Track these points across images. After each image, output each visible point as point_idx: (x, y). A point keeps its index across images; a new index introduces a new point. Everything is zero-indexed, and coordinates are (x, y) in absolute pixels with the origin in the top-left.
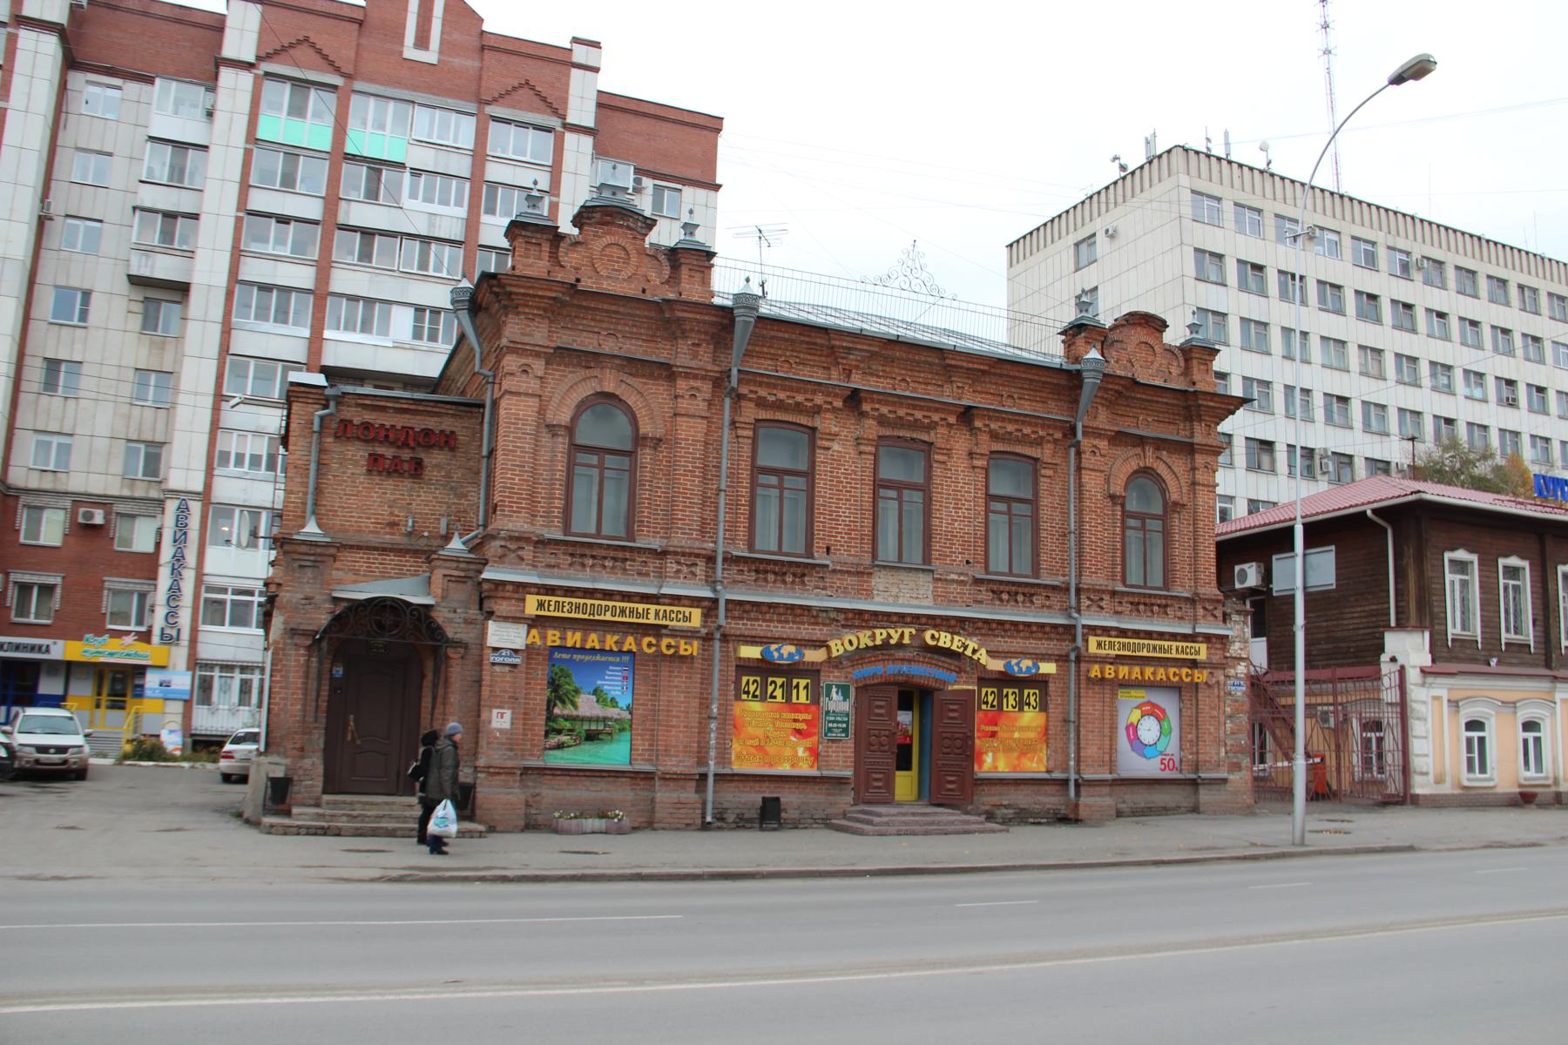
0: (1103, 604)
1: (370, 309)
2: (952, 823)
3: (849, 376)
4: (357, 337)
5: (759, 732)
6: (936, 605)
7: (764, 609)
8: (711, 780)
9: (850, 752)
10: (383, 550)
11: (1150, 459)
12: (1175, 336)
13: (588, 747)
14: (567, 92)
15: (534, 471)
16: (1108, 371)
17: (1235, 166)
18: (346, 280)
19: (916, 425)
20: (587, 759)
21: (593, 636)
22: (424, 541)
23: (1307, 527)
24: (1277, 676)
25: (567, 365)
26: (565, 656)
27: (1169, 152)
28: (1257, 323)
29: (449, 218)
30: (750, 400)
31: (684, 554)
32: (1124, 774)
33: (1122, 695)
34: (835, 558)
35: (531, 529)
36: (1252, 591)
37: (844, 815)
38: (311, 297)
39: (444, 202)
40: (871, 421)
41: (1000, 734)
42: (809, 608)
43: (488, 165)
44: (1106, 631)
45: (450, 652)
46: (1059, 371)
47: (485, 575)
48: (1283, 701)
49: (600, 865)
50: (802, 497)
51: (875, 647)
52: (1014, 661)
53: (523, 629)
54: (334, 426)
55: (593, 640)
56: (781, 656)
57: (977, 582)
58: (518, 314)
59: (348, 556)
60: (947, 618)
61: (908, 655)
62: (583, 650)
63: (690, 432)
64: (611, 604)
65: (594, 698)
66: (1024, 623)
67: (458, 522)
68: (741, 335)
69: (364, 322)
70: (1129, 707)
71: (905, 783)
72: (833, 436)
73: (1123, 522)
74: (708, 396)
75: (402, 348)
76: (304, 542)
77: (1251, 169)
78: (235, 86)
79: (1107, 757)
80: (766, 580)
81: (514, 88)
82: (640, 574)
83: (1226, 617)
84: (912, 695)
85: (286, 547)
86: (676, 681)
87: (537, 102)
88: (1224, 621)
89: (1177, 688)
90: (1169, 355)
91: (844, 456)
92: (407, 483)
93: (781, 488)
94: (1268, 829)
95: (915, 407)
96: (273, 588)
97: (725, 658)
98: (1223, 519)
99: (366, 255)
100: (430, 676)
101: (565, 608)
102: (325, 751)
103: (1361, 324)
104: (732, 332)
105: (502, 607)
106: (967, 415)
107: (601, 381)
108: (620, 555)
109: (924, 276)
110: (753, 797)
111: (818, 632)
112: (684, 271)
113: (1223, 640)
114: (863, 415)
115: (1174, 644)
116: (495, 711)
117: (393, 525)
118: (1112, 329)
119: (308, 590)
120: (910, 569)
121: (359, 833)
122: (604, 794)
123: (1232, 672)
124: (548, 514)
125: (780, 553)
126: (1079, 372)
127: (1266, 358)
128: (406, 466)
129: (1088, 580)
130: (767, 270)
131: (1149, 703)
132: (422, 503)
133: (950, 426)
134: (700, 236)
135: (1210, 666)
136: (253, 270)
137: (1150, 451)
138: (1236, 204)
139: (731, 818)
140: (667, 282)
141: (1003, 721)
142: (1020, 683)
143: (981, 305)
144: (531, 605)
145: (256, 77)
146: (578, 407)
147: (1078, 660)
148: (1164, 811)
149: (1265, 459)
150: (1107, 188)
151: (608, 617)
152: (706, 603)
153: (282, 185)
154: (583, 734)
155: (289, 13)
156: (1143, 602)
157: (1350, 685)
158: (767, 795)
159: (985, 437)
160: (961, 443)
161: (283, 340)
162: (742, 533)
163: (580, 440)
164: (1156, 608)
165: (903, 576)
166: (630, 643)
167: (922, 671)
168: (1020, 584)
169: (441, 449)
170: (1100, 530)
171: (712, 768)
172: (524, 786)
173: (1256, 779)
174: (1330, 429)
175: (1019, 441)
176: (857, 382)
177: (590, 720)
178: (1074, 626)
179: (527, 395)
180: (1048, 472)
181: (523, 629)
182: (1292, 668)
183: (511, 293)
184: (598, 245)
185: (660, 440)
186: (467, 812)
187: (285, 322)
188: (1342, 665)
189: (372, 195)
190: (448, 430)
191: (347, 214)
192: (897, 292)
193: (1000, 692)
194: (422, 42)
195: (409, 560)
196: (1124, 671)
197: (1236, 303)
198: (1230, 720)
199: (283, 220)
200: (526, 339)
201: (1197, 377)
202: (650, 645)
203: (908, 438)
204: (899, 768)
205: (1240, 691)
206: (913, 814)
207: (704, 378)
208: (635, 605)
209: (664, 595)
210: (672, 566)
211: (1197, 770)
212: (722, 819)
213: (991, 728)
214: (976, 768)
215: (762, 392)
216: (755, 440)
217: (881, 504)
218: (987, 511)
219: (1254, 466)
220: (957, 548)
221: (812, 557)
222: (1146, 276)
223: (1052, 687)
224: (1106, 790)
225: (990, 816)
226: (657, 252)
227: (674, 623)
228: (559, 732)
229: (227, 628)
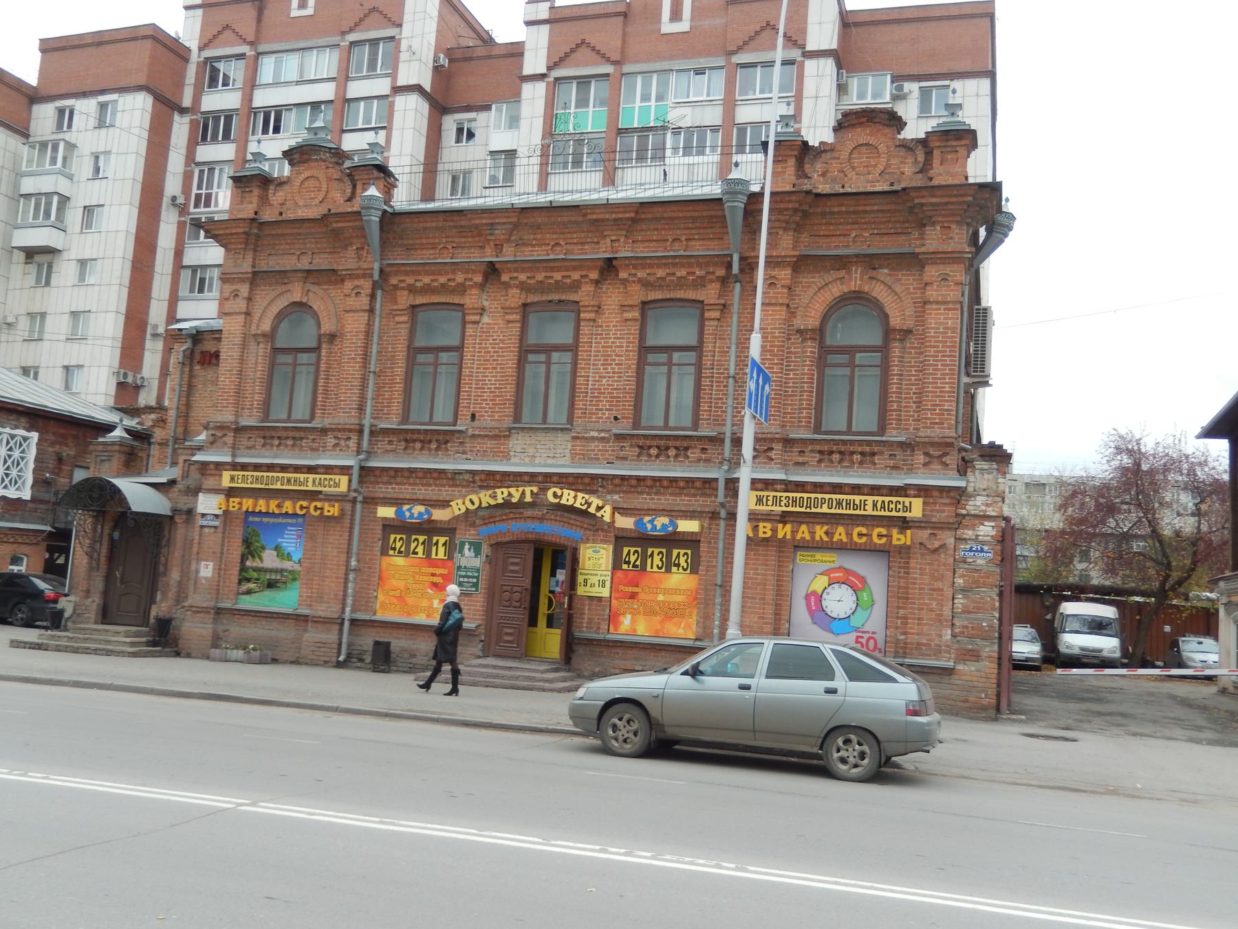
5: (401, 584)
6: (572, 465)
11: (856, 280)
13: (268, 593)
14: (806, 22)
26: (257, 519)
30: (403, 289)
31: (339, 430)
41: (642, 596)
52: (647, 519)
53: (222, 497)
56: (654, 527)
63: (355, 324)
65: (275, 553)
78: (534, 96)
81: (757, 33)
82: (312, 449)
86: (331, 539)
87: (598, 57)
95: (552, 269)
101: (246, 480)
105: (210, 482)
106: (609, 267)
108: (297, 434)
114: (506, 286)
122: (273, 633)
131: (840, 569)
141: (645, 581)
144: (226, 480)
145: (548, 83)
151: (825, 509)
155: (569, 24)
159: (635, 288)
162: (396, 407)
177: (271, 571)
193: (645, 552)
194: (676, 15)
206: (495, 667)
213: (630, 589)
220: (604, 404)
226: (907, 146)
227: (327, 489)
228: (249, 580)
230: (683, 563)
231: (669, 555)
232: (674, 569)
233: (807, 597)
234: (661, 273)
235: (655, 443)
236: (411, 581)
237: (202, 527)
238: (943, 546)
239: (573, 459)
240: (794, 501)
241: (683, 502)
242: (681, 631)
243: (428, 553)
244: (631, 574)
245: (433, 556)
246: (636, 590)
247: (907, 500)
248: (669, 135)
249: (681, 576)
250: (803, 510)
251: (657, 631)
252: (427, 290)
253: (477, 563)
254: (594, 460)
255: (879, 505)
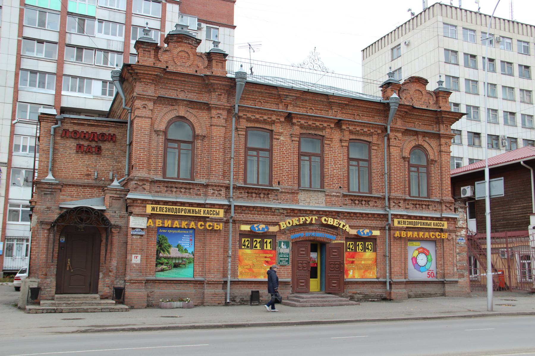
0: (400, 205)
1: (82, 82)
2: (335, 301)
3: (287, 107)
4: (77, 94)
5: (250, 263)
7: (251, 209)
8: (229, 284)
9: (290, 271)
10: (84, 186)
11: (182, 111)
12: (431, 87)
13: (174, 270)
15: (149, 151)
16: (402, 103)
17: (463, 11)
18: (70, 69)
19: (316, 128)
20: (174, 275)
21: (176, 222)
22: (103, 182)
23: (491, 170)
24: (480, 236)
25: (163, 104)
26: (164, 231)
27: (433, 6)
28: (473, 81)
29: (116, 41)
30: (244, 118)
31: (216, 186)
32: (411, 279)
33: (409, 244)
34: (282, 187)
35: (149, 176)
36: (469, 198)
37: (288, 298)
38: (55, 76)
39: (114, 34)
40: (297, 127)
41: (356, 262)
42: (271, 208)
43: (133, 18)
44: (402, 216)
45: (113, 230)
46: (380, 103)
47: (128, 196)
48: (483, 247)
49: (177, 322)
50: (267, 160)
51: (300, 225)
52: (361, 230)
53: (145, 219)
54: (61, 132)
55: (176, 224)
56: (259, 229)
57: (345, 196)
58: (141, 82)
59: (68, 189)
60: (332, 212)
61: (314, 228)
62: (172, 228)
63: (218, 132)
64: (184, 208)
65: (177, 249)
66: (366, 214)
67: (118, 173)
68: (239, 90)
69: (79, 88)
70: (413, 250)
71: (314, 284)
72: (280, 134)
73: (409, 169)
74: (225, 117)
75: (95, 99)
76: (46, 183)
77: (471, 12)
79: (403, 272)
80: (252, 196)
82: (197, 195)
83: (455, 210)
84: (317, 246)
85: (38, 186)
88: (455, 211)
89: (434, 241)
90: (429, 95)
91: (285, 141)
92: (95, 157)
93: (258, 157)
94: (476, 304)
95: (316, 120)
96: (33, 204)
97: (234, 231)
98: (457, 167)
99: (79, 58)
100: (104, 241)
101: (164, 210)
102: (57, 275)
103: (521, 80)
104: (235, 89)
105: (136, 210)
106: (339, 123)
107: (178, 112)
108: (188, 186)
109: (319, 63)
110: (247, 291)
111: (275, 219)
112: (214, 62)
113: (455, 219)
114: (293, 124)
115: (432, 222)
116: (133, 256)
117: (88, 175)
118: (404, 84)
119: (48, 204)
120: (304, 190)
121: (71, 311)
122: (182, 291)
123: (459, 234)
124: (156, 169)
125: (258, 185)
126: (388, 103)
127: (476, 96)
128: (94, 150)
129: (393, 194)
130: (252, 62)
132: (101, 165)
133: (331, 128)
134: (221, 47)
135: (449, 231)
136: (26, 64)
137: (420, 138)
138: (464, 28)
139: (238, 300)
140: (207, 67)
141: (357, 256)
142: (364, 239)
143: (351, 77)
144: (149, 209)
146: (168, 122)
147: (390, 229)
148: (430, 295)
149: (477, 141)
150: (405, 23)
151: (183, 214)
152: (226, 207)
153: (39, 26)
154: (173, 265)
156: (418, 204)
157: (514, 239)
158: (254, 290)
159: (347, 133)
160: (336, 135)
161: (42, 96)
162: (241, 177)
163: (169, 137)
164: (424, 206)
165: (312, 194)
166: (192, 225)
167: (321, 235)
168: (363, 197)
169: (109, 142)
170: (399, 173)
171: (229, 278)
172: (146, 287)
173: (471, 281)
174: (506, 127)
175: (362, 135)
176: (290, 110)
177: (176, 258)
178: (388, 215)
179: (145, 117)
180: (375, 148)
181: (145, 219)
182: (485, 232)
183: (137, 73)
184: (175, 51)
185: (205, 137)
186: (121, 300)
187: (44, 87)
188: (510, 231)
189: (81, 30)
190: (112, 133)
191: (70, 39)
192: (308, 70)
195: (96, 191)
196: (410, 234)
197: (463, 72)
198: (458, 255)
199: (40, 42)
200: (145, 93)
201: (441, 104)
202: (201, 225)
203: (313, 133)
204: (311, 277)
205: (463, 242)
206: (318, 297)
207: (223, 109)
208: (195, 208)
209: (207, 204)
210: (210, 191)
211: (444, 277)
212: (234, 301)
213: (351, 260)
214: (345, 277)
215: (249, 115)
216: (246, 136)
217: (302, 163)
218: (349, 165)
219: (471, 144)
220: (335, 181)
221: (272, 186)
222: (423, 62)
223: (378, 241)
224: (403, 286)
225: (352, 298)
226: (200, 56)
227: (212, 216)
228: (162, 264)
229: (20, 222)
230: (370, 248)
231: (365, 244)
232: (367, 250)
233: (412, 259)
234: (358, 129)
235: (358, 199)
236: (255, 261)
237: (133, 235)
238: (453, 238)
239: (326, 204)
240: (169, 209)
241: (374, 223)
242: (371, 275)
243: (262, 247)
244: (351, 253)
245: (265, 248)
246: (353, 260)
247: (443, 222)
248: (96, 22)
249: (369, 253)
250: (173, 214)
251: (363, 276)
252: (257, 121)
253: (287, 251)
254: (334, 205)
255: (206, 212)
